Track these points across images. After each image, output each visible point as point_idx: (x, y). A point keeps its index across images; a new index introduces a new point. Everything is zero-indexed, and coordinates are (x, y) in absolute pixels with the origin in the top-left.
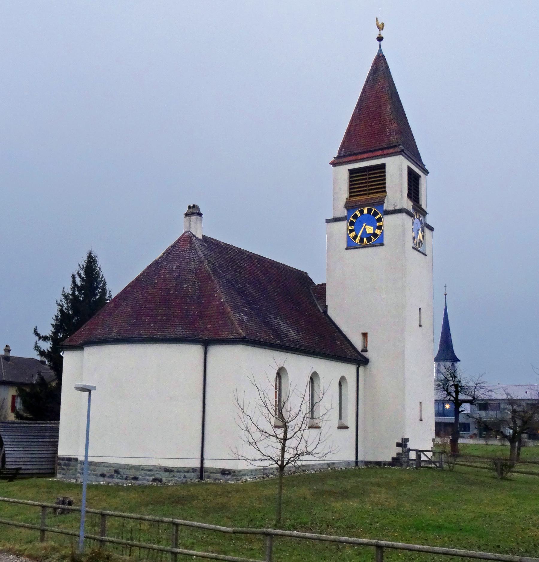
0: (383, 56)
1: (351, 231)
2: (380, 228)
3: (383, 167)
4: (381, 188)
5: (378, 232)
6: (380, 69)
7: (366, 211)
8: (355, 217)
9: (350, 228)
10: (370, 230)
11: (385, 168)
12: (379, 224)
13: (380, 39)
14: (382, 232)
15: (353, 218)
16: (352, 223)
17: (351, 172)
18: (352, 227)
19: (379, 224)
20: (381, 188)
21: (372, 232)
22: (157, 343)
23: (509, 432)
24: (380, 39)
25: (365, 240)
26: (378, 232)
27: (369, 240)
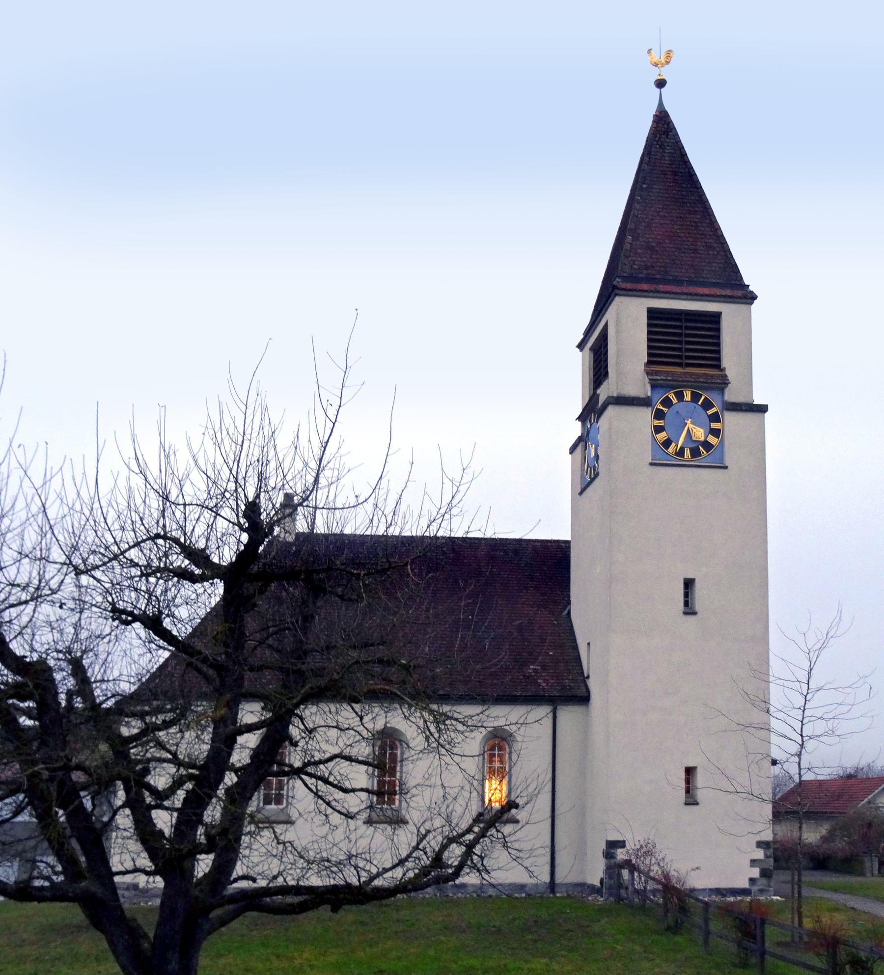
0: (666, 112)
1: (658, 429)
2: (716, 433)
3: (715, 319)
4: (656, 326)
5: (712, 440)
6: (663, 130)
7: (688, 396)
8: (667, 402)
9: (657, 423)
10: (699, 433)
11: (718, 322)
12: (714, 425)
13: (661, 84)
14: (722, 443)
15: (662, 403)
16: (659, 415)
17: (653, 314)
18: (661, 423)
19: (714, 425)
20: (656, 326)
21: (702, 439)
22: (461, 704)
23: (130, 728)
24: (661, 84)
25: (687, 453)
26: (712, 440)
27: (695, 453)
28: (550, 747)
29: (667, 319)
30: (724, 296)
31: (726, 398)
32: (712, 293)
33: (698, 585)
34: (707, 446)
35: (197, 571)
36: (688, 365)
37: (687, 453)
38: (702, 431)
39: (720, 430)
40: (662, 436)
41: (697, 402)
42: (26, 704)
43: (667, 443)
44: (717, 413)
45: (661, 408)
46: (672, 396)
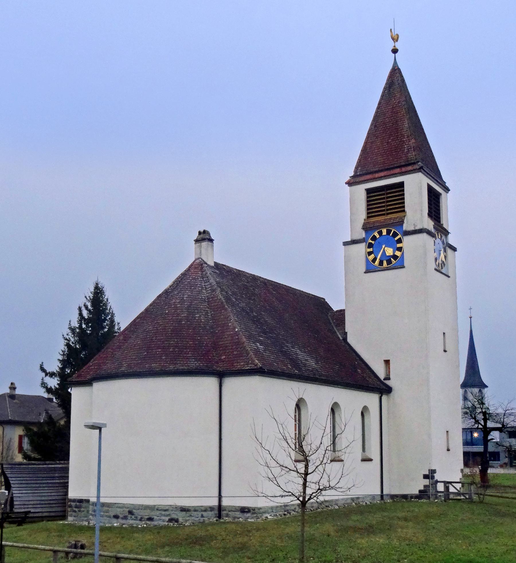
1: (370, 253)
2: (400, 249)
5: (398, 253)
10: (389, 252)
13: (395, 51)
15: (372, 239)
16: (370, 246)
19: (399, 245)
21: (392, 254)
24: (395, 51)
25: (385, 263)
26: (398, 253)
27: (389, 262)
28: (217, 411)
29: (395, 188)
30: (414, 170)
31: (404, 229)
32: (380, 176)
33: (446, 334)
34: (395, 257)
35: (312, 363)
36: (388, 214)
37: (385, 263)
38: (392, 250)
39: (402, 247)
40: (372, 257)
41: (389, 235)
42: (422, 501)
43: (374, 260)
44: (400, 238)
45: (371, 242)
46: (376, 234)
